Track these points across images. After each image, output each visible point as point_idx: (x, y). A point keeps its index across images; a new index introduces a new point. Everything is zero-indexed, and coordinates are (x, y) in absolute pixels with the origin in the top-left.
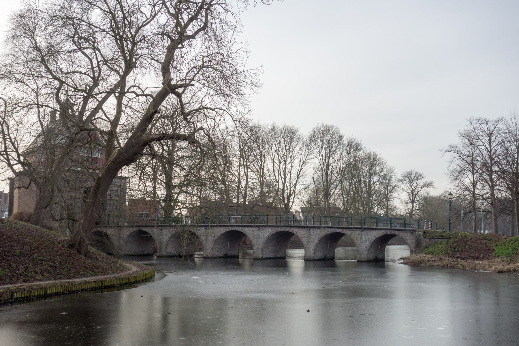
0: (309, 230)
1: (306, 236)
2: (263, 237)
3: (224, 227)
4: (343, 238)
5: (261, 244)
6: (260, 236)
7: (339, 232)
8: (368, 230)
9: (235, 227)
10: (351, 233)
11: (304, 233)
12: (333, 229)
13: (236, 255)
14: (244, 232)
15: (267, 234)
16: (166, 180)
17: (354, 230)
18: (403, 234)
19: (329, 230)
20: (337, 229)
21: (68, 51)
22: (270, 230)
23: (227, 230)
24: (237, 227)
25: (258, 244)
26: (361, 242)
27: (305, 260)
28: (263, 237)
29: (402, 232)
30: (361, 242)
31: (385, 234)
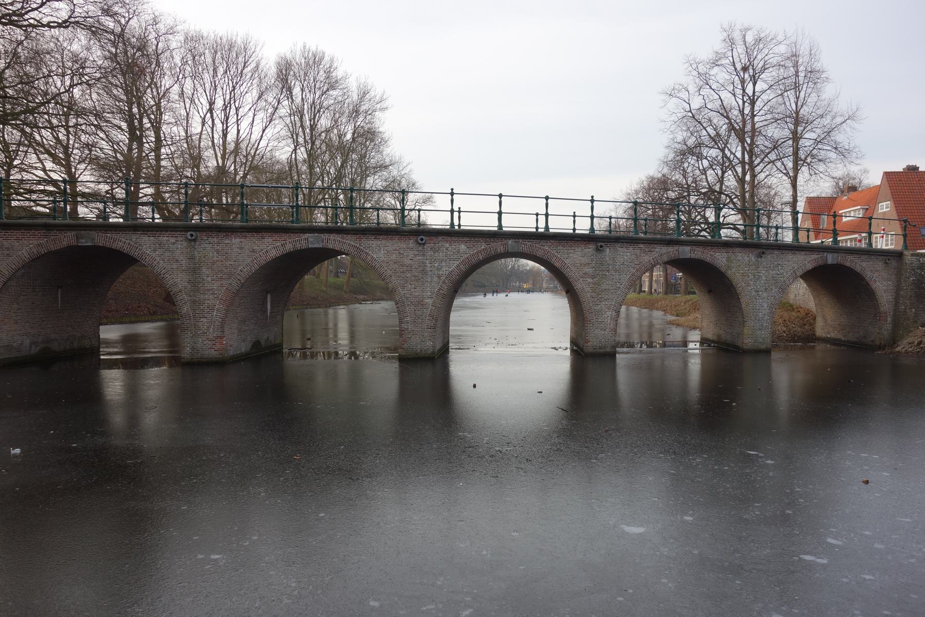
0: (599, 250)
1: (589, 270)
2: (439, 277)
3: (276, 237)
4: (130, 271)
5: (430, 301)
6: (424, 272)
7: (693, 256)
8: (776, 252)
9: (325, 236)
10: (728, 259)
11: (585, 260)
12: (676, 248)
13: (278, 342)
14: (135, 254)
15: (454, 265)
16: (160, 133)
17: (737, 250)
18: (864, 264)
19: (664, 249)
20: (688, 249)
21: (111, 16)
22: (463, 247)
23: (289, 247)
24: (332, 237)
25: (420, 303)
26: (757, 291)
27: (402, 360)
28: (439, 277)
29: (863, 257)
30: (757, 291)
31: (821, 263)
